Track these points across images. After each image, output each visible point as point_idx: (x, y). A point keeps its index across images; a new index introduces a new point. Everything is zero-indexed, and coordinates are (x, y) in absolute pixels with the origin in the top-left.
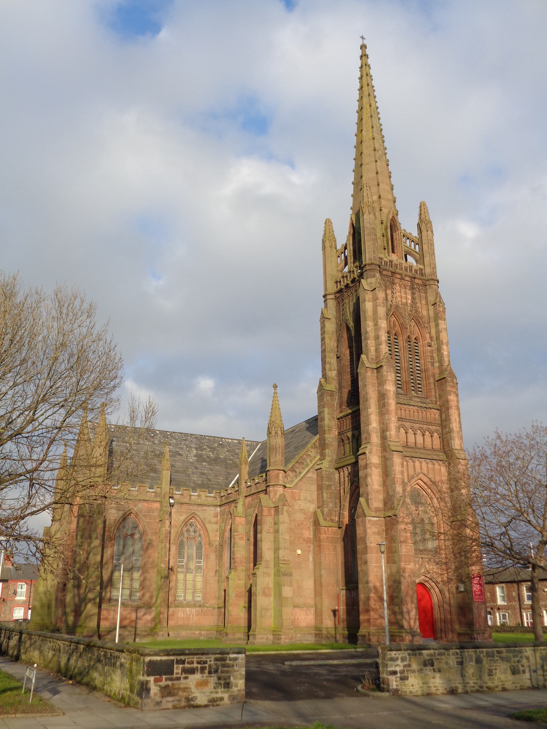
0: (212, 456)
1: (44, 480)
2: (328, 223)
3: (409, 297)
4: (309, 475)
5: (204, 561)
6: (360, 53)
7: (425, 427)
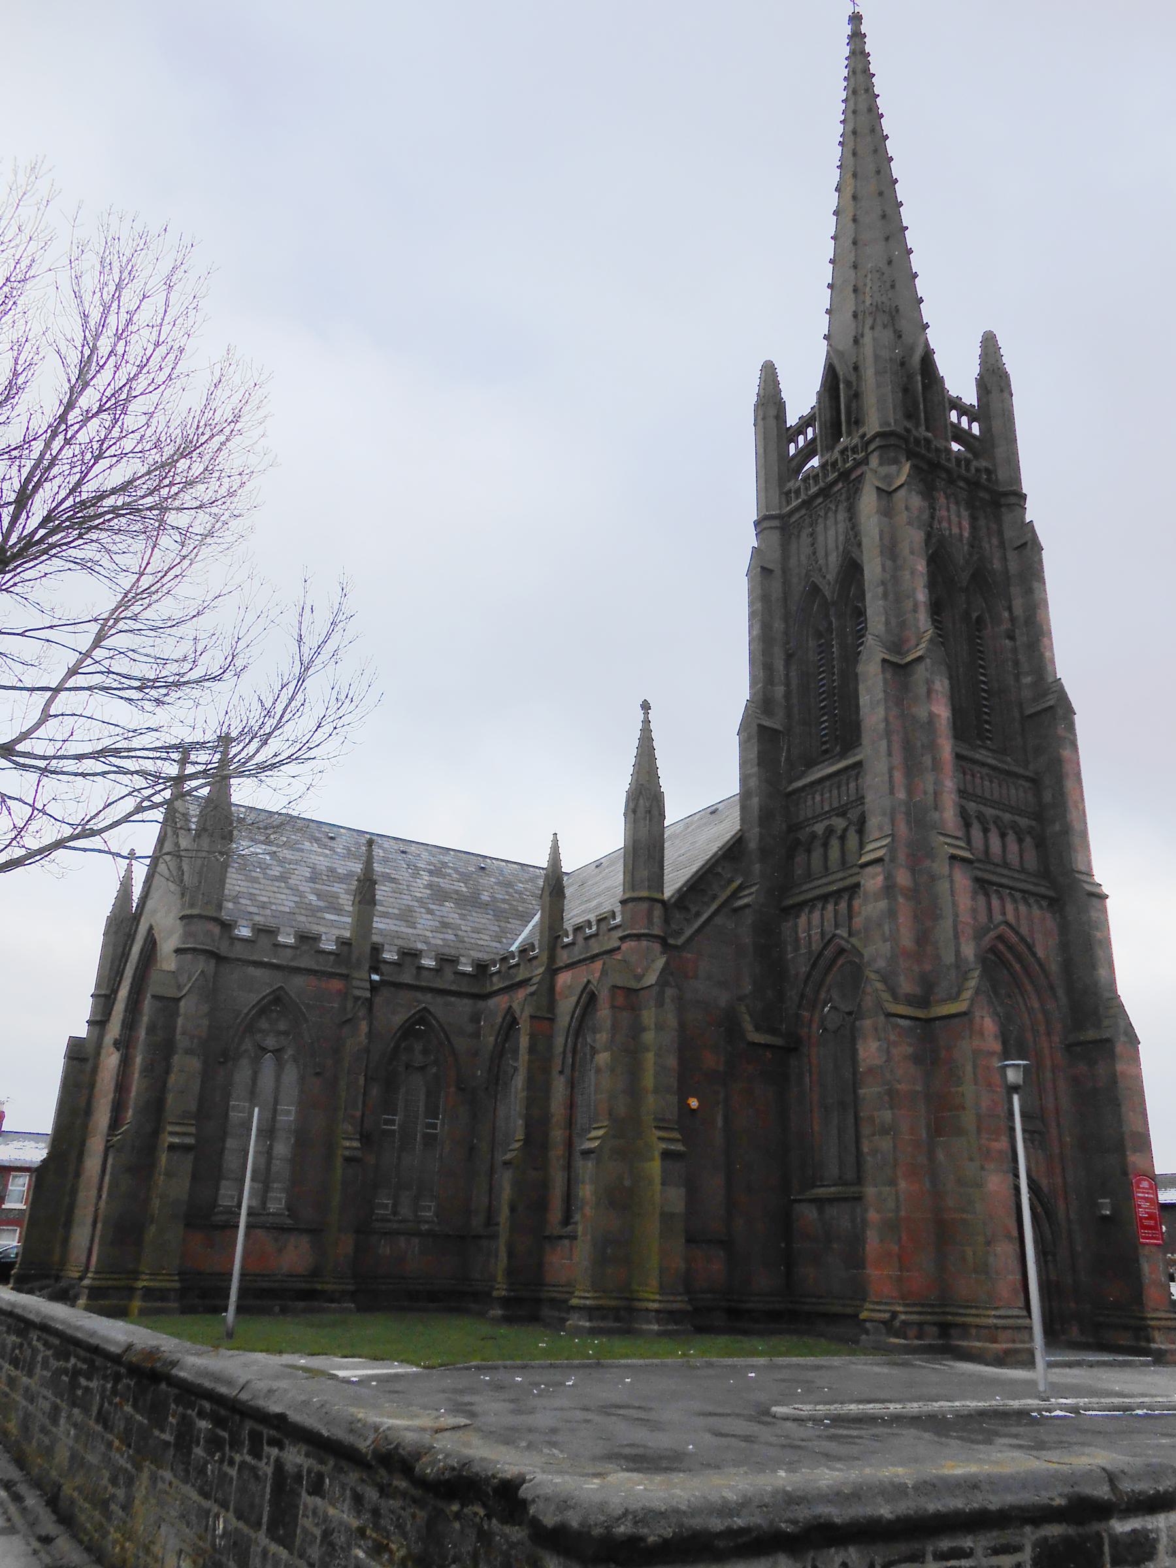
0: (464, 889)
1: (129, 591)
2: (769, 373)
3: (966, 524)
4: (718, 920)
5: (443, 1125)
6: (848, 30)
7: (1007, 817)
